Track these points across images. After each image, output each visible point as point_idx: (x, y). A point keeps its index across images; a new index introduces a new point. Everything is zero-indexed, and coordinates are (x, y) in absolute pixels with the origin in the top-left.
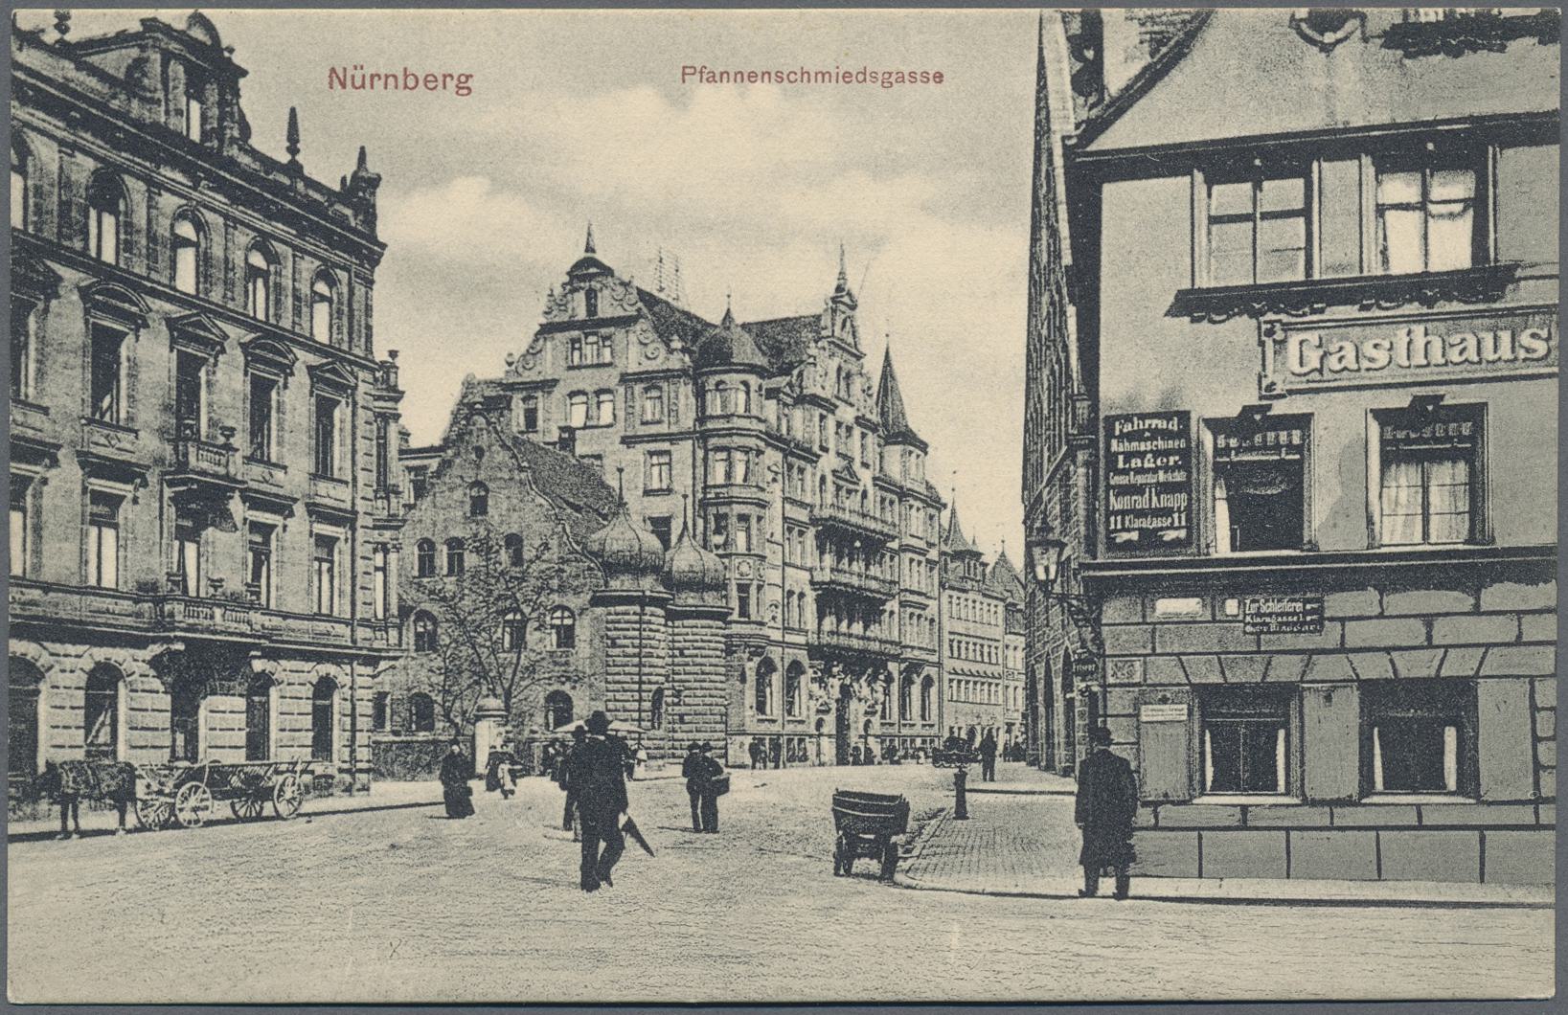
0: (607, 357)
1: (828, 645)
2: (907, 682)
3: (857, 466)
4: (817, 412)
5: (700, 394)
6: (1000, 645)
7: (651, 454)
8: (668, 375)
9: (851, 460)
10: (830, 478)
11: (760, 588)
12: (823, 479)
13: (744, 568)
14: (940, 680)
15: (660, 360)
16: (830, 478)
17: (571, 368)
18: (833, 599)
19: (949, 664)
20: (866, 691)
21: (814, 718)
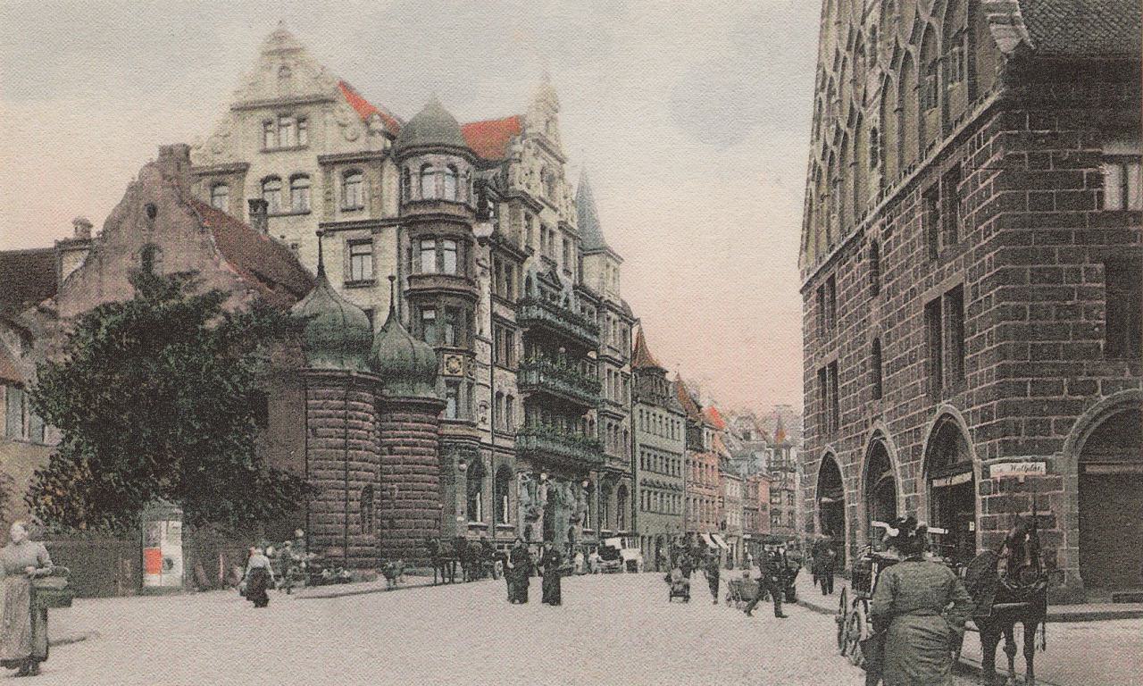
0: (304, 141)
1: (537, 448)
2: (606, 489)
3: (559, 271)
4: (523, 210)
5: (406, 179)
6: (683, 460)
7: (352, 243)
8: (366, 158)
9: (554, 265)
10: (535, 282)
11: (470, 386)
12: (529, 281)
13: (454, 365)
14: (634, 491)
15: (362, 140)
16: (535, 282)
17: (266, 151)
18: (537, 400)
19: (640, 475)
20: (570, 499)
21: (522, 525)
